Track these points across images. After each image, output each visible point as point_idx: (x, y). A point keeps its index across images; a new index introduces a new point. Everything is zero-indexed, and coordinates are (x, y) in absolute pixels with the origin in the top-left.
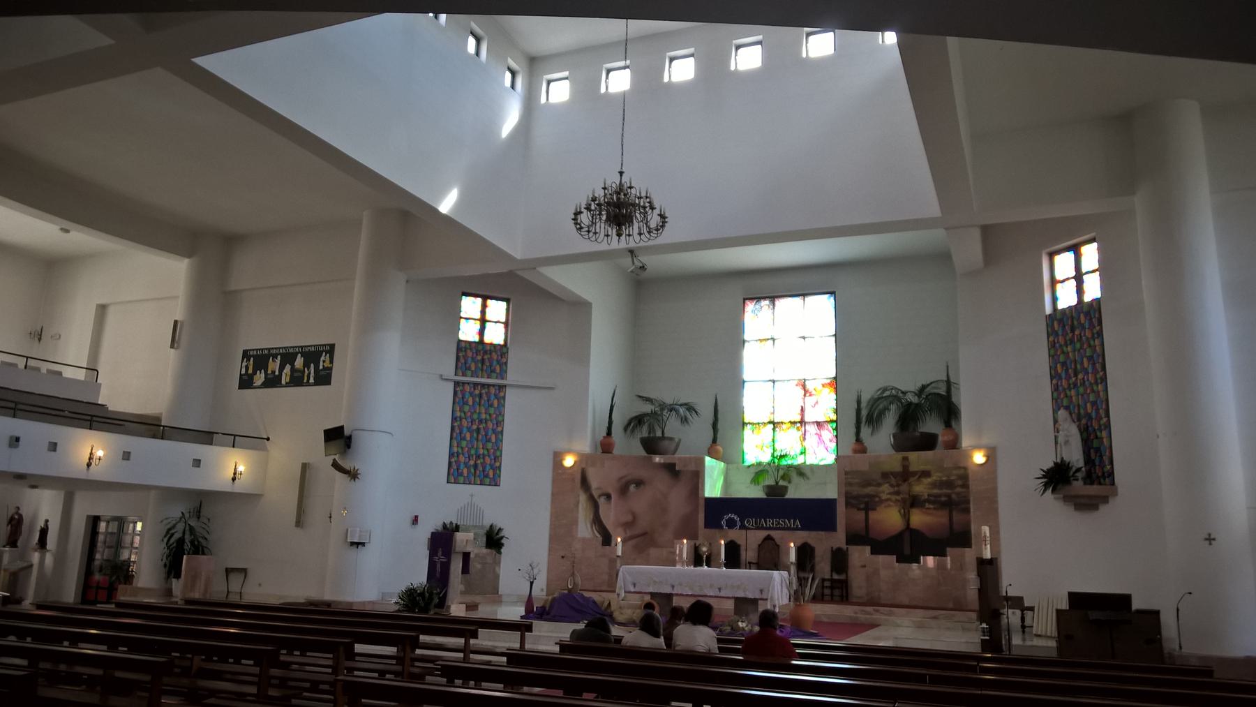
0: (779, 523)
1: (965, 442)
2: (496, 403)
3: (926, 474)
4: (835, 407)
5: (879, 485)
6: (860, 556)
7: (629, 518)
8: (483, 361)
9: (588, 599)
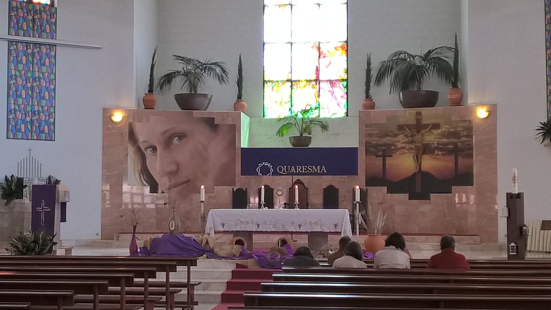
0: (307, 169)
1: (470, 100)
3: (436, 126)
4: (346, 68)
5: (396, 135)
7: (173, 168)
8: (34, 20)
9: (189, 238)
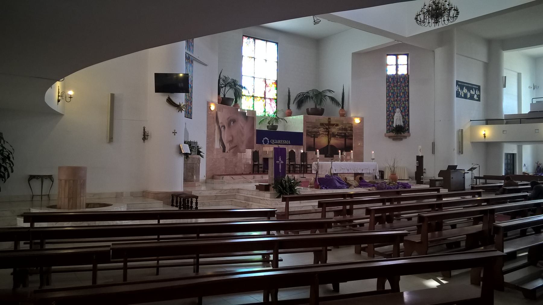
0: (283, 142)
2: (390, 95)
3: (337, 125)
5: (319, 128)
7: (231, 138)
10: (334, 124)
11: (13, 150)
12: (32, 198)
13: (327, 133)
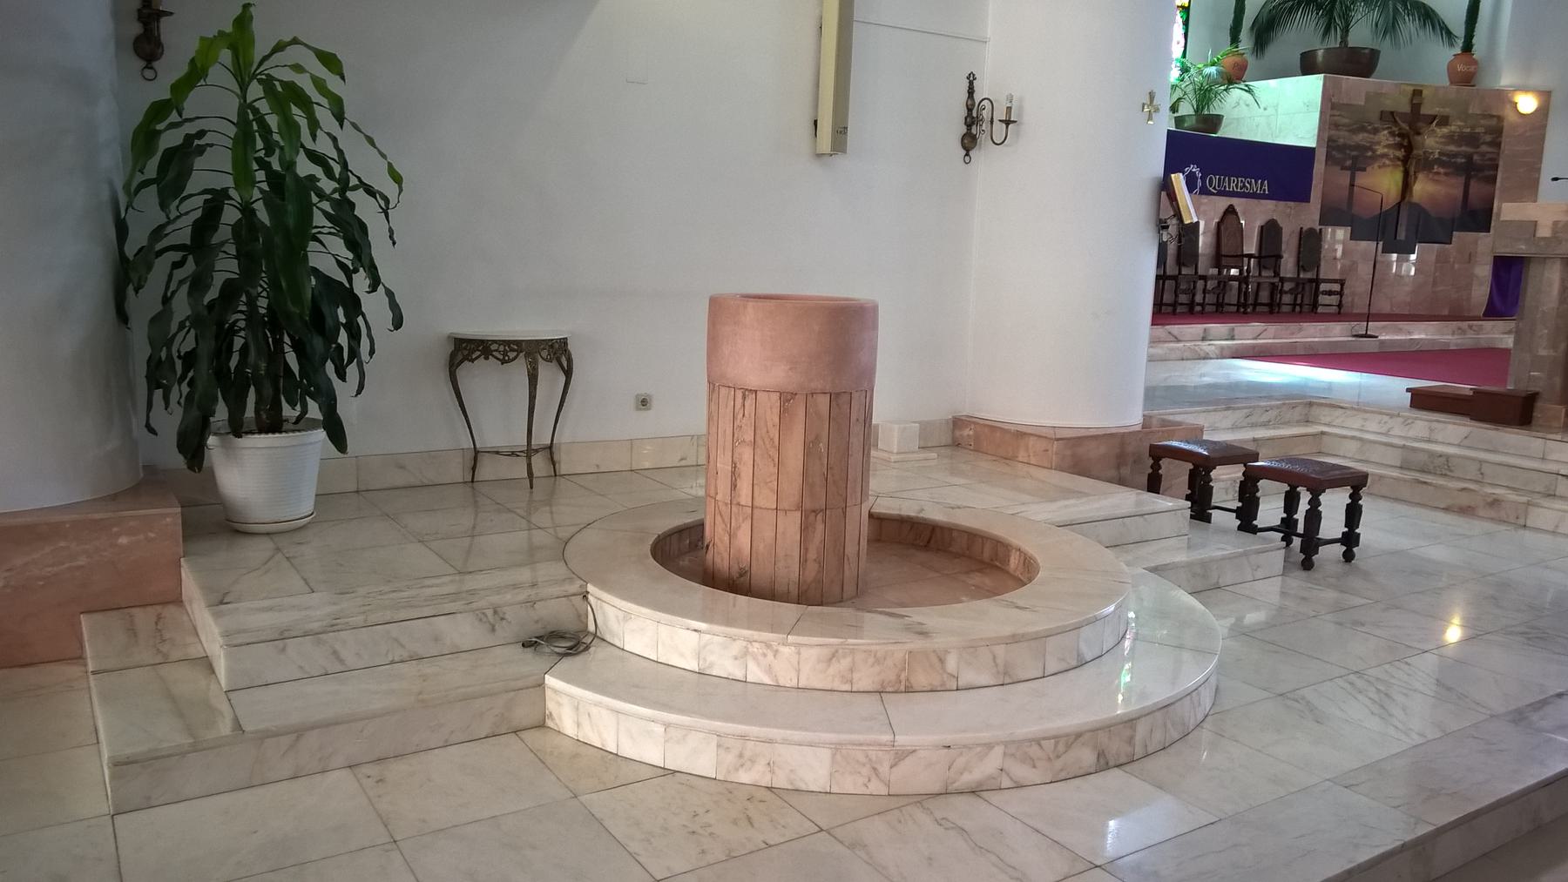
0: (1244, 186)
3: (1444, 121)
5: (1376, 131)
6: (1337, 238)
10: (1434, 117)
11: (397, 179)
12: (474, 469)
13: (1400, 153)
